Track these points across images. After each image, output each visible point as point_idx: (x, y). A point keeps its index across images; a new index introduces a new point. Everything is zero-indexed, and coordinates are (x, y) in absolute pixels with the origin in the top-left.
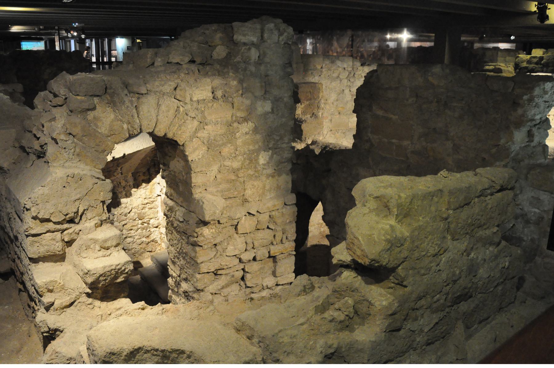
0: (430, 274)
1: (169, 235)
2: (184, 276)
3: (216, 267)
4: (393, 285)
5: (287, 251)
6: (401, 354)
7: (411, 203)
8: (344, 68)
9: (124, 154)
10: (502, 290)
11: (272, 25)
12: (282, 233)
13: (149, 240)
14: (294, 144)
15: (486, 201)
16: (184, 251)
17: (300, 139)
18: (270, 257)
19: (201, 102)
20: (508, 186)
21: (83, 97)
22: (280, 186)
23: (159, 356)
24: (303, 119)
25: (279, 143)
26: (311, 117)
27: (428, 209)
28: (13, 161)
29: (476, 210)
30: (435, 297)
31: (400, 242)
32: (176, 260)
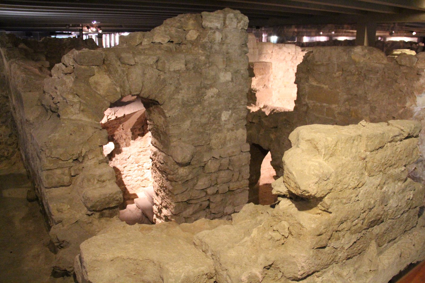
0: (351, 203)
1: (154, 173)
2: (164, 204)
4: (320, 211)
6: (326, 267)
7: (336, 145)
8: (289, 53)
9: (124, 115)
10: (407, 217)
11: (231, 15)
12: (239, 173)
13: (143, 178)
14: (249, 108)
15: (396, 145)
16: (164, 185)
17: (255, 104)
20: (414, 134)
21: (86, 67)
24: (257, 89)
25: (237, 105)
26: (263, 88)
27: (349, 150)
28: (37, 116)
29: (389, 152)
30: (354, 222)
31: (327, 176)
32: (159, 192)
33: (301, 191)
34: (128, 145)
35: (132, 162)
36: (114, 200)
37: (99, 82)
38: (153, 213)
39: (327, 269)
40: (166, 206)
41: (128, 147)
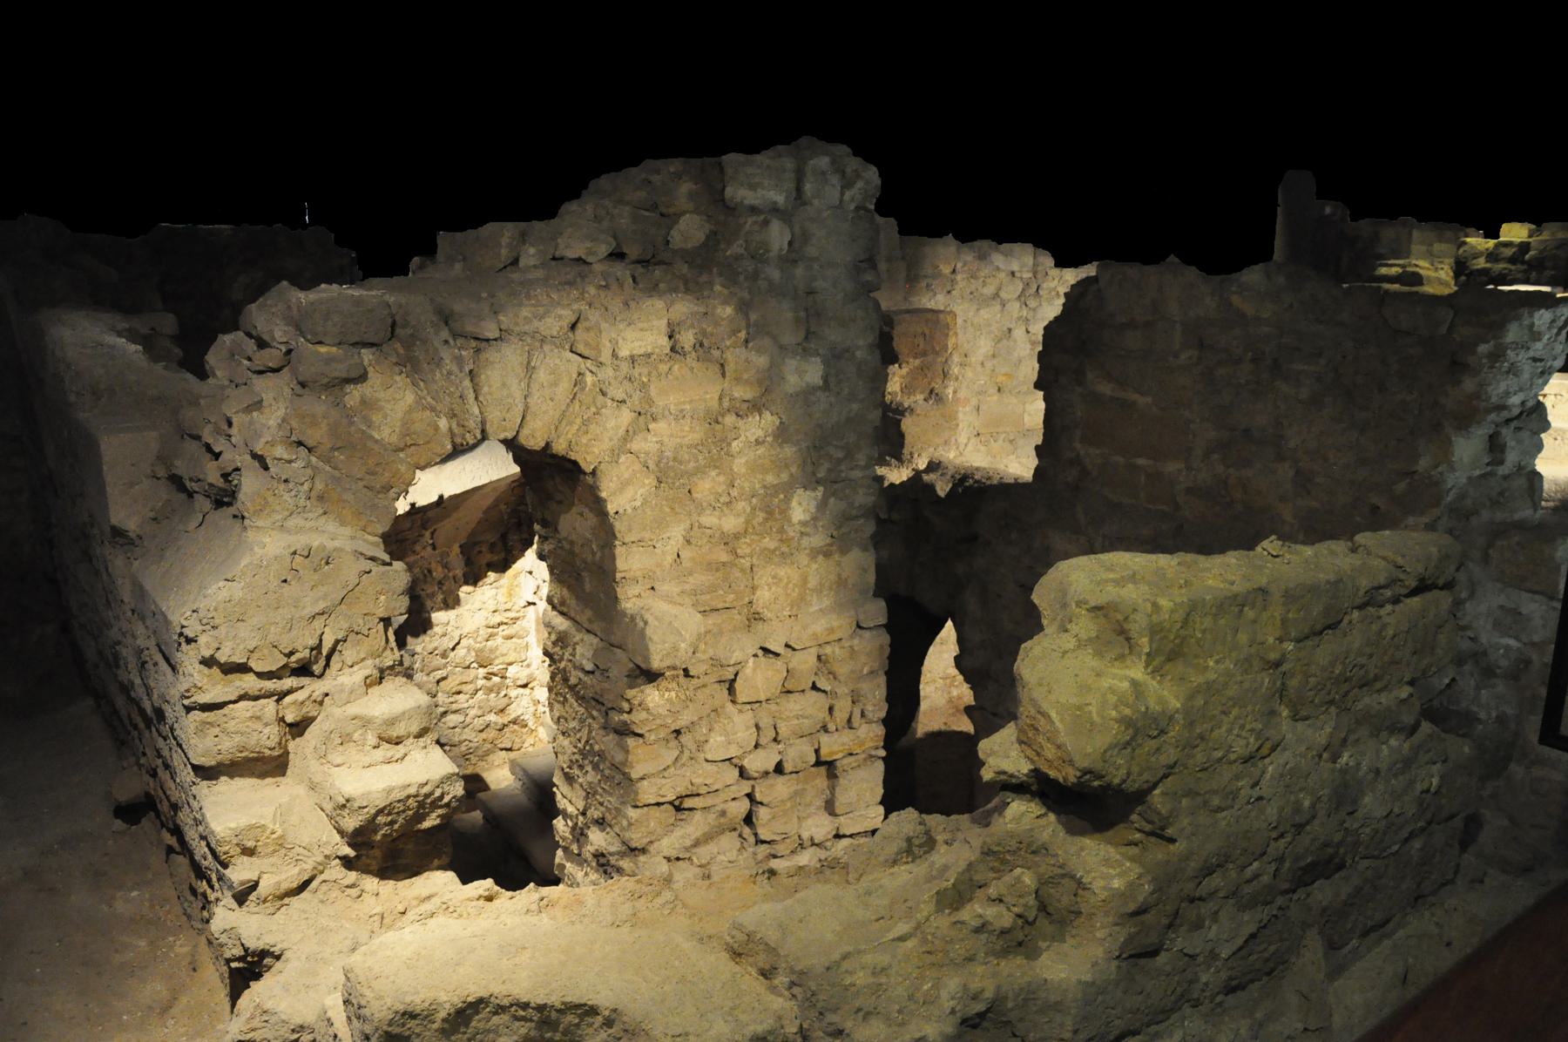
1: (557, 706)
2: (595, 813)
3: (679, 789)
4: (1138, 836)
5: (863, 748)
6: (1161, 1017)
7: (1185, 622)
8: (1013, 274)
9: (441, 497)
10: (1422, 849)
11: (823, 162)
14: (881, 471)
16: (597, 748)
17: (899, 458)
18: (818, 763)
20: (1438, 578)
23: (531, 1020)
24: (906, 405)
26: (925, 400)
29: (1356, 640)
31: (1158, 725)
32: (576, 771)
33: (1078, 774)
34: (451, 602)
35: (468, 663)
36: (435, 805)
37: (380, 400)
38: (557, 845)
39: (1166, 1023)
40: (603, 819)
41: (453, 608)
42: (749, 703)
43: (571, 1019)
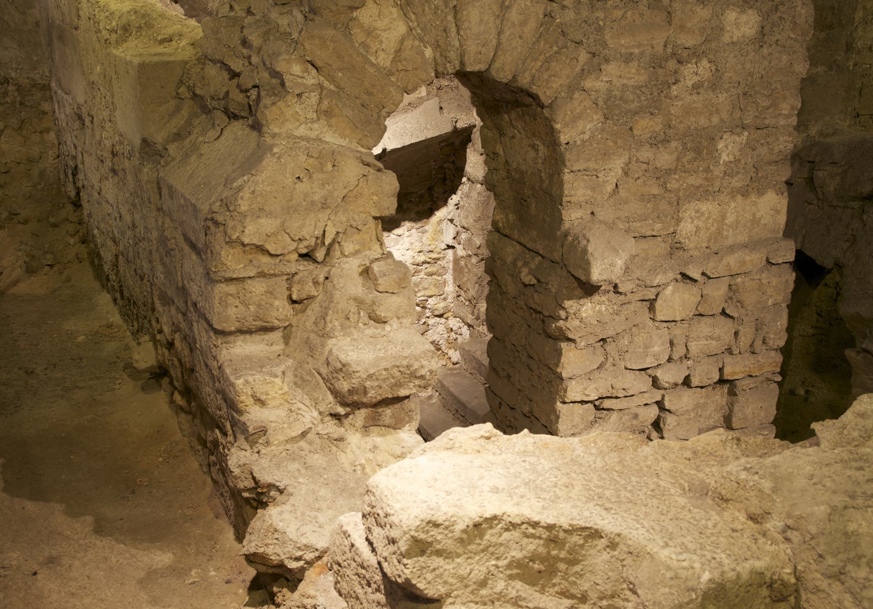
3: (601, 391)
5: (762, 372)
18: (722, 381)
19: (598, 6)
22: (760, 219)
23: (540, 538)
37: (375, 29)
42: (666, 322)
43: (576, 539)
